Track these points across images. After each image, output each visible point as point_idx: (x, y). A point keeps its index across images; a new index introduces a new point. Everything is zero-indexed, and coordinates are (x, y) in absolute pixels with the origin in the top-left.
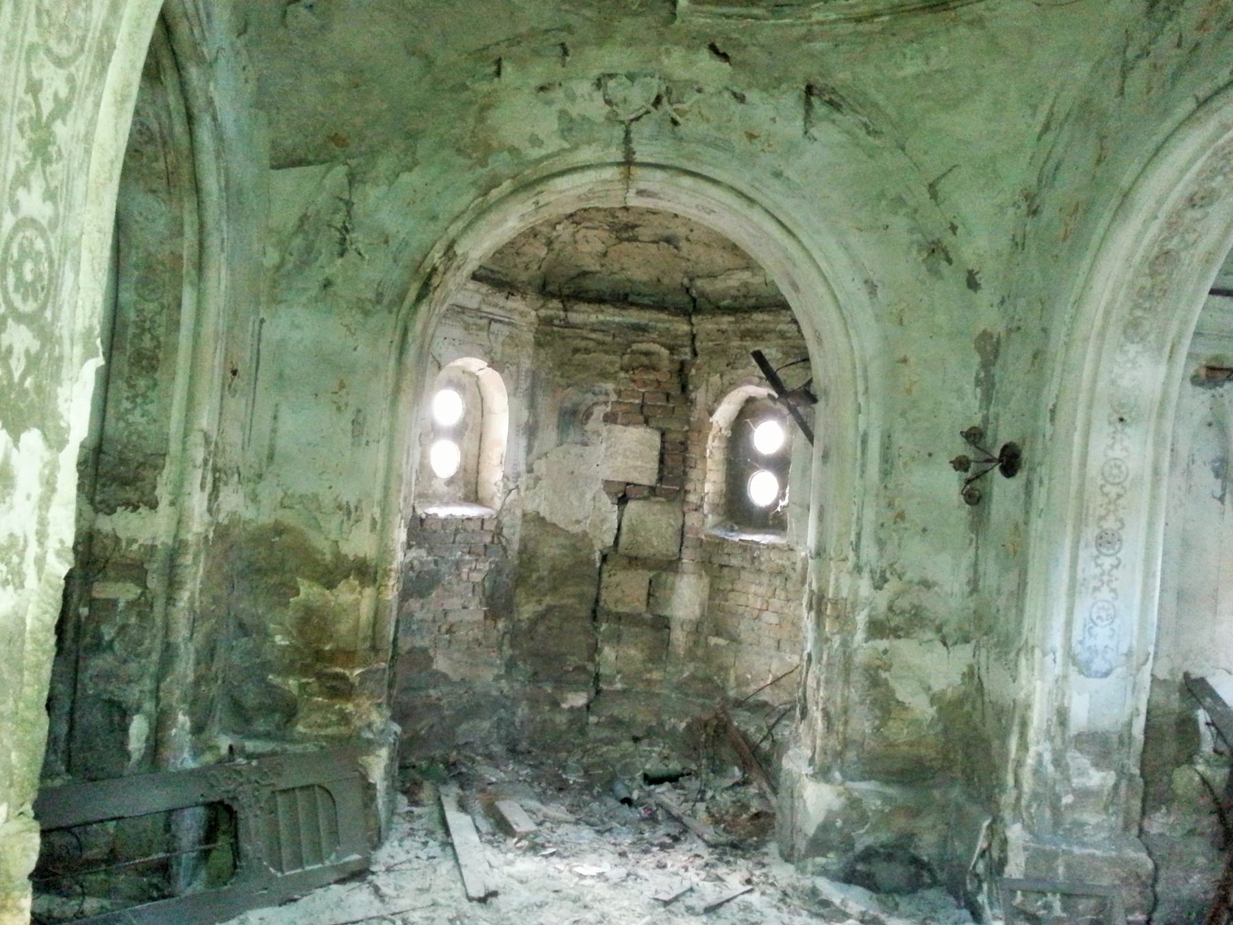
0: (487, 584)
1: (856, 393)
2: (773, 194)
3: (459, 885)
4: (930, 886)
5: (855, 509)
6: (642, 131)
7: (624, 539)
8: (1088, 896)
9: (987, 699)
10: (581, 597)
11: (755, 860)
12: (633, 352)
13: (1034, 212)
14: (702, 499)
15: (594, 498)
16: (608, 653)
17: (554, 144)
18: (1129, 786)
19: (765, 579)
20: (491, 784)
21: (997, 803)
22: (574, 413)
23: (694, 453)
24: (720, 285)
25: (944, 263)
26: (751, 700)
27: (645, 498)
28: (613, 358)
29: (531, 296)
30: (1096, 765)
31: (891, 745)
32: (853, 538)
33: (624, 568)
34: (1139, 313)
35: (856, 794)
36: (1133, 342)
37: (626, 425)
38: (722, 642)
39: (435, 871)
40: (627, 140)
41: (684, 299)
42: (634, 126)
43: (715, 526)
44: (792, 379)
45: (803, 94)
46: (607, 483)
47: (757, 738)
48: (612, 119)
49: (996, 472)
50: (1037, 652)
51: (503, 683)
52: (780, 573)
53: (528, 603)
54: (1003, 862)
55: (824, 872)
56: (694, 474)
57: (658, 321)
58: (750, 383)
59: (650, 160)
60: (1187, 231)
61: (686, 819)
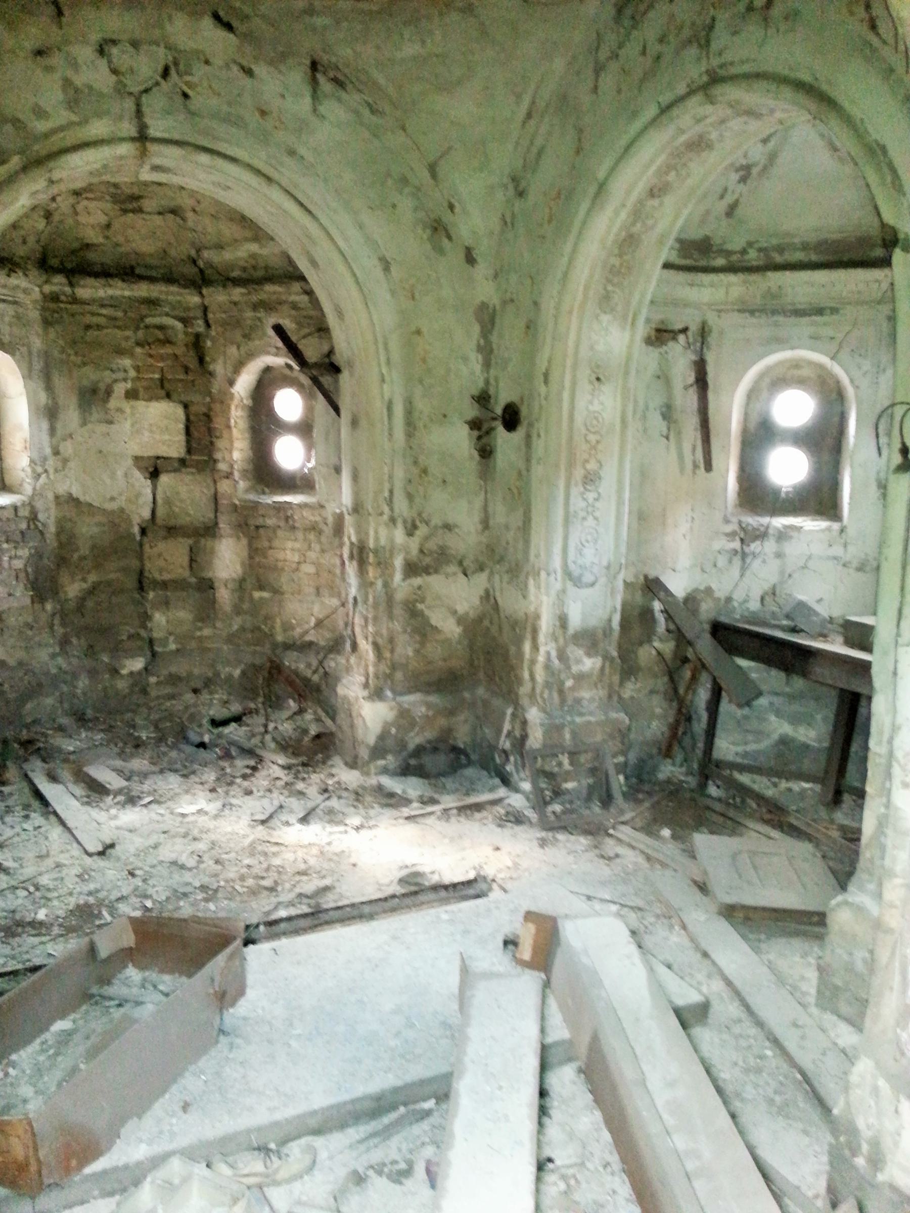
0: (30, 570)
1: (379, 365)
2: (288, 173)
3: (75, 845)
4: (466, 766)
5: (386, 470)
6: (154, 104)
7: (160, 512)
8: (586, 752)
9: (502, 615)
10: (125, 570)
11: (326, 772)
12: (147, 327)
13: (521, 194)
14: (232, 467)
15: (126, 475)
16: (159, 618)
17: (63, 116)
18: (611, 666)
19: (300, 535)
20: (70, 753)
21: (517, 694)
22: (94, 391)
23: (218, 423)
24: (228, 256)
25: (445, 241)
26: (298, 643)
27: (175, 471)
28: (128, 333)
29: (34, 273)
30: (589, 655)
31: (430, 663)
32: (386, 494)
33: (165, 538)
34: (610, 288)
35: (406, 706)
36: (605, 312)
37: (150, 399)
38: (265, 595)
39: (47, 838)
40: (139, 113)
41: (190, 271)
42: (144, 99)
43: (247, 491)
44: (312, 350)
45: (309, 70)
46: (137, 459)
47: (308, 673)
48: (120, 90)
49: (500, 430)
50: (543, 574)
51: (60, 660)
52: (314, 528)
53: (73, 581)
54: (524, 737)
55: (385, 771)
56: (221, 444)
57: (167, 293)
58: (268, 353)
59: (166, 135)
60: (647, 218)
61: (259, 751)
